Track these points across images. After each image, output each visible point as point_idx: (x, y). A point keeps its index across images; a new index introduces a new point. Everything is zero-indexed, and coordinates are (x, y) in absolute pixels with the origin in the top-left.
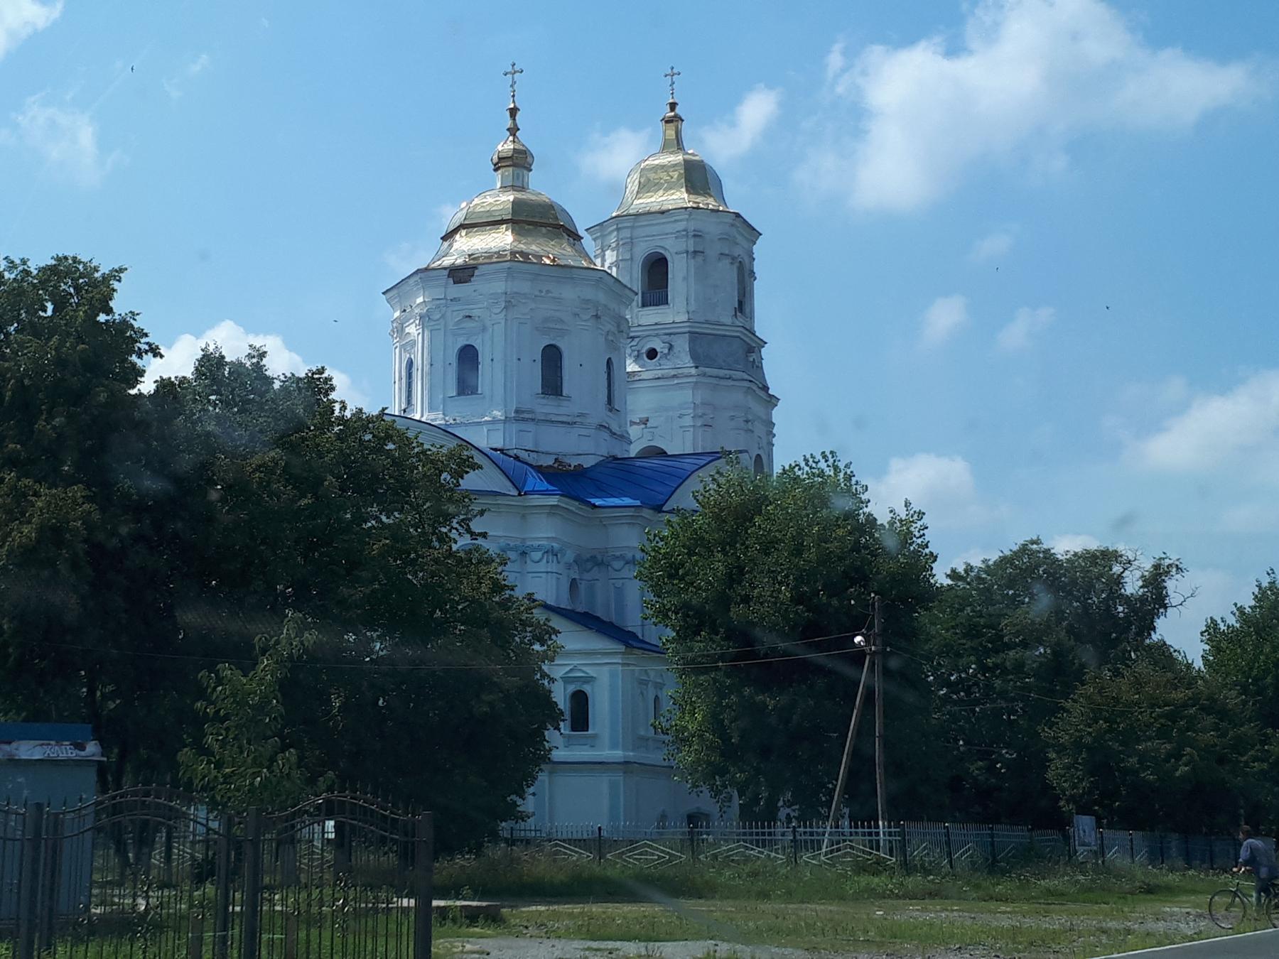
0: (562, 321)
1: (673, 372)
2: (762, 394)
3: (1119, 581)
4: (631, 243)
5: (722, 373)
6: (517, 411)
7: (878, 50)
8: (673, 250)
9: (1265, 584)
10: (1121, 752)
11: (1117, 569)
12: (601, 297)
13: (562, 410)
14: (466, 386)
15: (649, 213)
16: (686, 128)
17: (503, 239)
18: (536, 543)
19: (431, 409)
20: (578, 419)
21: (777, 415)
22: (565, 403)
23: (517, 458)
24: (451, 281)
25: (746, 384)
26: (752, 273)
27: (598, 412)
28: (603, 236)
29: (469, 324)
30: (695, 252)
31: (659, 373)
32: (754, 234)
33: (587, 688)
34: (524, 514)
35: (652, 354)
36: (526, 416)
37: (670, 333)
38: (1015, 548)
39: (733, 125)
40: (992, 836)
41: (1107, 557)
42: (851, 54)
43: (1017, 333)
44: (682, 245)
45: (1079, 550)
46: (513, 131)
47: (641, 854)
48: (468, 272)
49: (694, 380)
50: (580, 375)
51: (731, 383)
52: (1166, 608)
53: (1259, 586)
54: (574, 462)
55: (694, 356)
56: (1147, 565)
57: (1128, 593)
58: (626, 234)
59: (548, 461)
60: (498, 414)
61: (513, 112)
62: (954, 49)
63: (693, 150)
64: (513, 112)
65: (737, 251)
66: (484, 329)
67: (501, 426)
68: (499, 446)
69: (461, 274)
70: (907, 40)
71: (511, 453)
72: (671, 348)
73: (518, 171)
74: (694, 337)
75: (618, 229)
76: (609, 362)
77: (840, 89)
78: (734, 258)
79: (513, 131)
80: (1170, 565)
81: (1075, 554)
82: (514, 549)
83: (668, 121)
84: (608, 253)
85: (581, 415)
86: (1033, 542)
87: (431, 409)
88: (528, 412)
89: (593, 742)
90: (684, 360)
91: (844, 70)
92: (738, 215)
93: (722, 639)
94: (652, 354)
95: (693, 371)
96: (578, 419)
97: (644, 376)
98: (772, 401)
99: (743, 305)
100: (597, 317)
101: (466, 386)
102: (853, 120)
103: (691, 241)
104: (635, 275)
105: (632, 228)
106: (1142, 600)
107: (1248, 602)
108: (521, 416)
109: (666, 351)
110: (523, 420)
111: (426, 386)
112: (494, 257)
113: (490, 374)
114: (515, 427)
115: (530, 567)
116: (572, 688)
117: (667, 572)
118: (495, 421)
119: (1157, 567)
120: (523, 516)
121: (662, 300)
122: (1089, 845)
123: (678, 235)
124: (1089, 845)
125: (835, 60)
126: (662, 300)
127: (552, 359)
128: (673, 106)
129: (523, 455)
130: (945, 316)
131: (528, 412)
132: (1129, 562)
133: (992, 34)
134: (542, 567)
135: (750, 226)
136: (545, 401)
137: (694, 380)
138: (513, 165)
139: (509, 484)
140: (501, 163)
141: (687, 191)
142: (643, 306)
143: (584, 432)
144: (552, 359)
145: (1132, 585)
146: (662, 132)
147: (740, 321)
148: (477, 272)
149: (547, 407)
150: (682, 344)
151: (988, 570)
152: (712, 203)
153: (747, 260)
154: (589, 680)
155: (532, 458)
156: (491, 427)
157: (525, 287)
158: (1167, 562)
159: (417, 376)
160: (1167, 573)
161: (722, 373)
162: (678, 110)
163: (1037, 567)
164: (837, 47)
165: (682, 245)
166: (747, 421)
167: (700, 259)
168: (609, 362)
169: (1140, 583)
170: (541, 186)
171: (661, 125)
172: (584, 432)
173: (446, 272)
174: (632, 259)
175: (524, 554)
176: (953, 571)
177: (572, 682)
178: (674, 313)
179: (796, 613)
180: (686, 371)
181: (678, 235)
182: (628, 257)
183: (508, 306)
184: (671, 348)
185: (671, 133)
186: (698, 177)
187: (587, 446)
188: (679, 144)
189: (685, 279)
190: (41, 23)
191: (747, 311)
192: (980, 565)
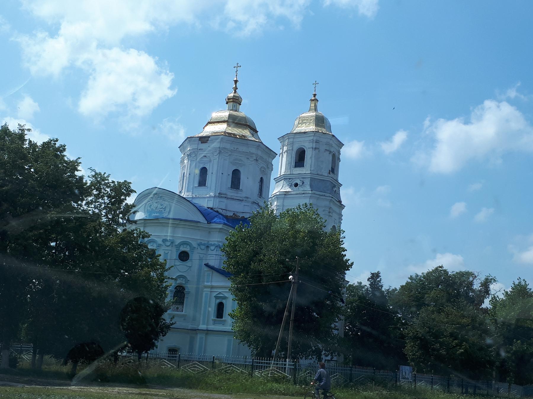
0: (240, 160)
1: (303, 192)
2: (338, 203)
3: (471, 284)
4: (293, 143)
5: (321, 193)
6: (219, 194)
7: (442, 120)
8: (307, 147)
9: (517, 283)
10: (433, 341)
11: (471, 279)
12: (259, 153)
13: (239, 195)
14: (202, 182)
15: (300, 133)
16: (319, 104)
17: (222, 127)
18: (213, 243)
19: (188, 191)
20: (244, 199)
21: (344, 212)
22: (240, 192)
23: (217, 212)
24: (200, 142)
25: (331, 198)
26: (339, 159)
27: (255, 196)
28: (284, 141)
29: (205, 159)
30: (316, 148)
31: (298, 192)
32: (341, 145)
33: (224, 301)
34: (210, 231)
35: (296, 185)
36: (223, 196)
37: (302, 177)
38: (433, 269)
39: (391, 142)
40: (351, 370)
41: (469, 274)
42: (432, 121)
43: (482, 216)
44: (311, 145)
45: (458, 271)
46: (236, 89)
47: (193, 367)
48: (207, 139)
49: (310, 195)
50: (248, 182)
51: (324, 197)
52: (489, 295)
53: (514, 284)
54: (241, 215)
55: (311, 186)
56: (483, 279)
57: (474, 288)
58: (291, 140)
59: (230, 214)
60: (212, 194)
61: (236, 82)
62: (467, 122)
63: (321, 112)
64: (236, 82)
65: (332, 150)
66: (210, 161)
67: (212, 199)
68: (211, 206)
69: (204, 140)
70: (450, 118)
71: (215, 210)
72: (303, 183)
73: (235, 104)
74: (312, 180)
75: (289, 138)
76: (262, 179)
77: (427, 132)
78: (330, 152)
79: (236, 89)
80: (491, 279)
81: (457, 273)
82: (204, 245)
83: (312, 100)
84: (285, 147)
85: (247, 198)
86: (440, 267)
87: (188, 191)
88: (224, 194)
89: (224, 323)
90: (308, 188)
91: (430, 126)
92: (333, 136)
93: (250, 278)
94: (296, 185)
95: (310, 192)
96: (244, 199)
97: (292, 193)
98: (342, 207)
99: (334, 170)
100: (257, 160)
101: (202, 182)
102: (432, 142)
103: (314, 144)
104: (293, 156)
105: (294, 138)
106: (480, 291)
107: (509, 290)
108: (221, 195)
109: (301, 184)
110: (221, 197)
111: (187, 182)
112: (216, 135)
113: (211, 179)
114: (218, 200)
115: (210, 252)
116: (218, 301)
117: (231, 250)
118: (210, 197)
119: (487, 279)
120: (210, 232)
121: (303, 166)
122: (408, 379)
123: (310, 141)
124: (408, 379)
125: (427, 123)
126: (303, 166)
127: (236, 174)
128: (315, 95)
129: (220, 211)
130: (459, 208)
131: (224, 194)
132: (476, 277)
133: (480, 118)
134: (214, 252)
135: (339, 141)
136: (230, 191)
137: (310, 195)
138: (233, 102)
139: (201, 216)
140: (229, 101)
141: (316, 126)
142: (295, 167)
143: (246, 204)
144: (236, 174)
145: (477, 286)
146: (309, 104)
147: (332, 175)
148: (210, 139)
149: (232, 193)
150: (307, 182)
151: (424, 277)
152: (324, 131)
153: (337, 154)
154: (225, 298)
155: (224, 213)
156: (209, 199)
157: (228, 146)
158: (491, 278)
159: (185, 178)
160: (491, 282)
161: (321, 193)
162: (316, 97)
163: (441, 276)
164: (428, 119)
165: (311, 145)
166: (329, 212)
167: (317, 151)
168: (262, 179)
169: (480, 285)
170: (243, 111)
171: (310, 102)
172: (246, 204)
173: (198, 139)
174: (292, 150)
175: (208, 247)
176: (411, 276)
177: (218, 299)
178: (305, 170)
179: (278, 267)
180: (308, 192)
181: (310, 141)
182: (291, 149)
183: (220, 153)
184: (303, 183)
185: (313, 105)
186: (320, 121)
187: (247, 209)
188: (316, 110)
189: (311, 158)
190: (170, 96)
191: (336, 173)
192: (421, 274)
